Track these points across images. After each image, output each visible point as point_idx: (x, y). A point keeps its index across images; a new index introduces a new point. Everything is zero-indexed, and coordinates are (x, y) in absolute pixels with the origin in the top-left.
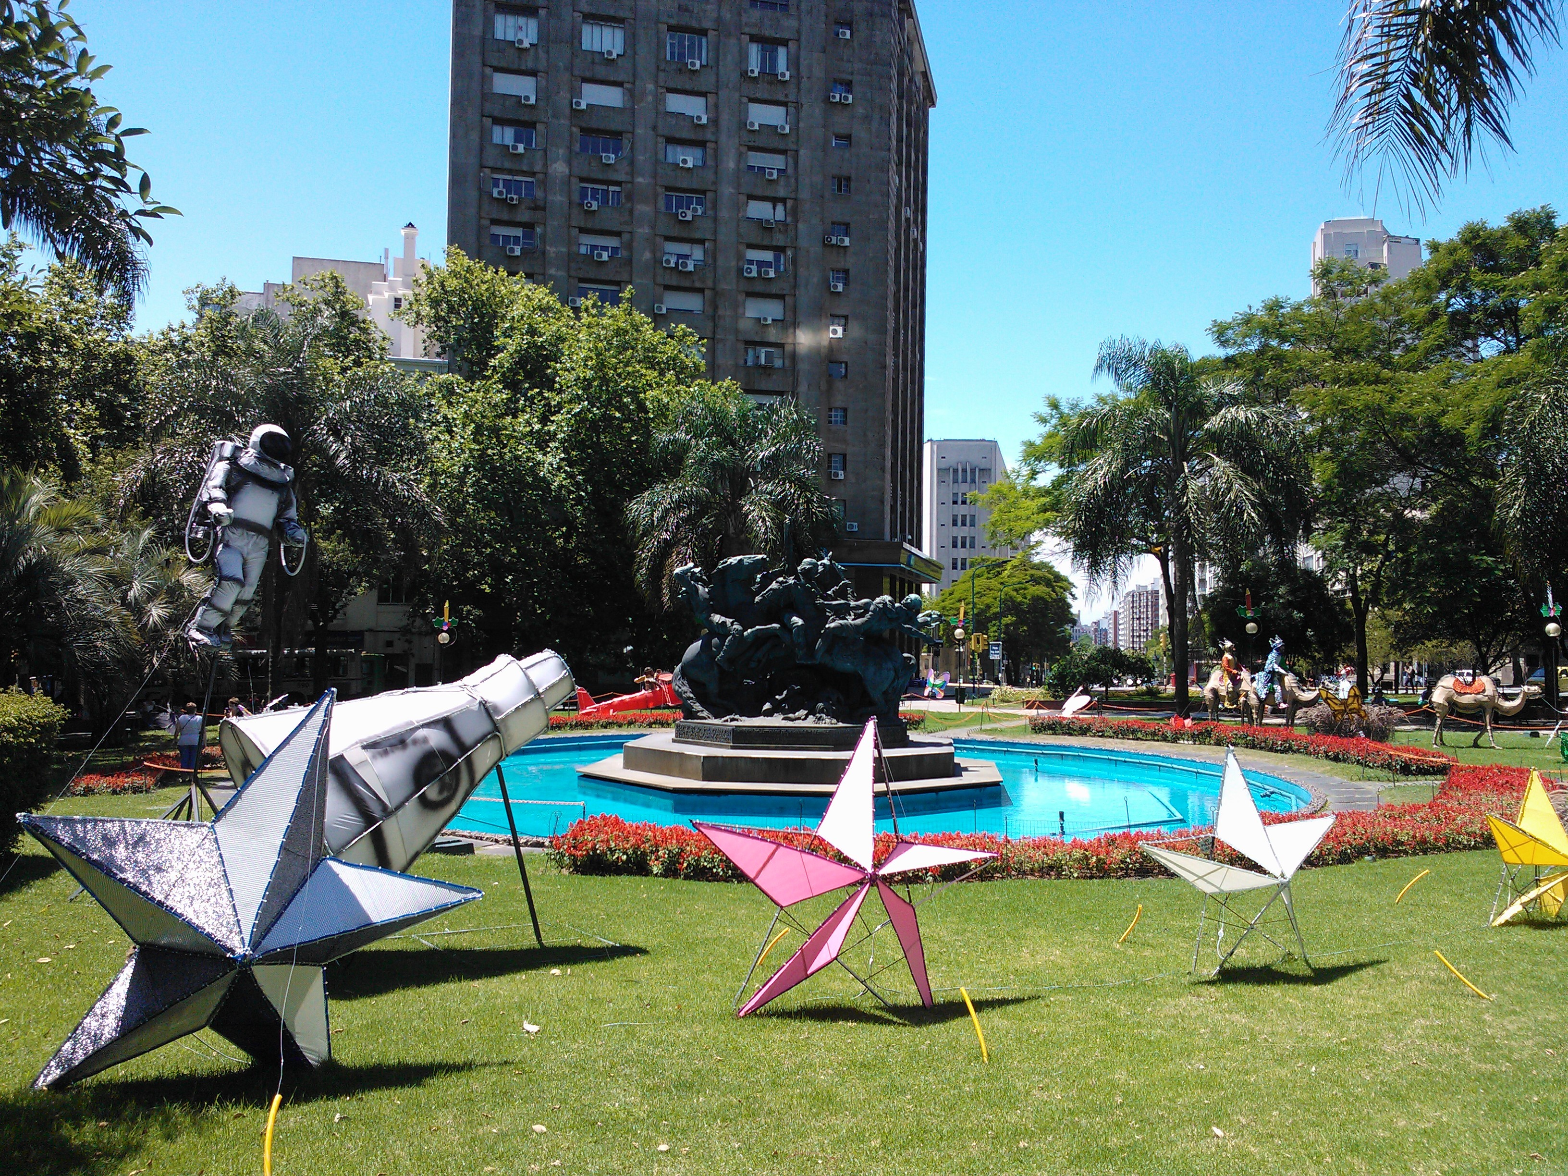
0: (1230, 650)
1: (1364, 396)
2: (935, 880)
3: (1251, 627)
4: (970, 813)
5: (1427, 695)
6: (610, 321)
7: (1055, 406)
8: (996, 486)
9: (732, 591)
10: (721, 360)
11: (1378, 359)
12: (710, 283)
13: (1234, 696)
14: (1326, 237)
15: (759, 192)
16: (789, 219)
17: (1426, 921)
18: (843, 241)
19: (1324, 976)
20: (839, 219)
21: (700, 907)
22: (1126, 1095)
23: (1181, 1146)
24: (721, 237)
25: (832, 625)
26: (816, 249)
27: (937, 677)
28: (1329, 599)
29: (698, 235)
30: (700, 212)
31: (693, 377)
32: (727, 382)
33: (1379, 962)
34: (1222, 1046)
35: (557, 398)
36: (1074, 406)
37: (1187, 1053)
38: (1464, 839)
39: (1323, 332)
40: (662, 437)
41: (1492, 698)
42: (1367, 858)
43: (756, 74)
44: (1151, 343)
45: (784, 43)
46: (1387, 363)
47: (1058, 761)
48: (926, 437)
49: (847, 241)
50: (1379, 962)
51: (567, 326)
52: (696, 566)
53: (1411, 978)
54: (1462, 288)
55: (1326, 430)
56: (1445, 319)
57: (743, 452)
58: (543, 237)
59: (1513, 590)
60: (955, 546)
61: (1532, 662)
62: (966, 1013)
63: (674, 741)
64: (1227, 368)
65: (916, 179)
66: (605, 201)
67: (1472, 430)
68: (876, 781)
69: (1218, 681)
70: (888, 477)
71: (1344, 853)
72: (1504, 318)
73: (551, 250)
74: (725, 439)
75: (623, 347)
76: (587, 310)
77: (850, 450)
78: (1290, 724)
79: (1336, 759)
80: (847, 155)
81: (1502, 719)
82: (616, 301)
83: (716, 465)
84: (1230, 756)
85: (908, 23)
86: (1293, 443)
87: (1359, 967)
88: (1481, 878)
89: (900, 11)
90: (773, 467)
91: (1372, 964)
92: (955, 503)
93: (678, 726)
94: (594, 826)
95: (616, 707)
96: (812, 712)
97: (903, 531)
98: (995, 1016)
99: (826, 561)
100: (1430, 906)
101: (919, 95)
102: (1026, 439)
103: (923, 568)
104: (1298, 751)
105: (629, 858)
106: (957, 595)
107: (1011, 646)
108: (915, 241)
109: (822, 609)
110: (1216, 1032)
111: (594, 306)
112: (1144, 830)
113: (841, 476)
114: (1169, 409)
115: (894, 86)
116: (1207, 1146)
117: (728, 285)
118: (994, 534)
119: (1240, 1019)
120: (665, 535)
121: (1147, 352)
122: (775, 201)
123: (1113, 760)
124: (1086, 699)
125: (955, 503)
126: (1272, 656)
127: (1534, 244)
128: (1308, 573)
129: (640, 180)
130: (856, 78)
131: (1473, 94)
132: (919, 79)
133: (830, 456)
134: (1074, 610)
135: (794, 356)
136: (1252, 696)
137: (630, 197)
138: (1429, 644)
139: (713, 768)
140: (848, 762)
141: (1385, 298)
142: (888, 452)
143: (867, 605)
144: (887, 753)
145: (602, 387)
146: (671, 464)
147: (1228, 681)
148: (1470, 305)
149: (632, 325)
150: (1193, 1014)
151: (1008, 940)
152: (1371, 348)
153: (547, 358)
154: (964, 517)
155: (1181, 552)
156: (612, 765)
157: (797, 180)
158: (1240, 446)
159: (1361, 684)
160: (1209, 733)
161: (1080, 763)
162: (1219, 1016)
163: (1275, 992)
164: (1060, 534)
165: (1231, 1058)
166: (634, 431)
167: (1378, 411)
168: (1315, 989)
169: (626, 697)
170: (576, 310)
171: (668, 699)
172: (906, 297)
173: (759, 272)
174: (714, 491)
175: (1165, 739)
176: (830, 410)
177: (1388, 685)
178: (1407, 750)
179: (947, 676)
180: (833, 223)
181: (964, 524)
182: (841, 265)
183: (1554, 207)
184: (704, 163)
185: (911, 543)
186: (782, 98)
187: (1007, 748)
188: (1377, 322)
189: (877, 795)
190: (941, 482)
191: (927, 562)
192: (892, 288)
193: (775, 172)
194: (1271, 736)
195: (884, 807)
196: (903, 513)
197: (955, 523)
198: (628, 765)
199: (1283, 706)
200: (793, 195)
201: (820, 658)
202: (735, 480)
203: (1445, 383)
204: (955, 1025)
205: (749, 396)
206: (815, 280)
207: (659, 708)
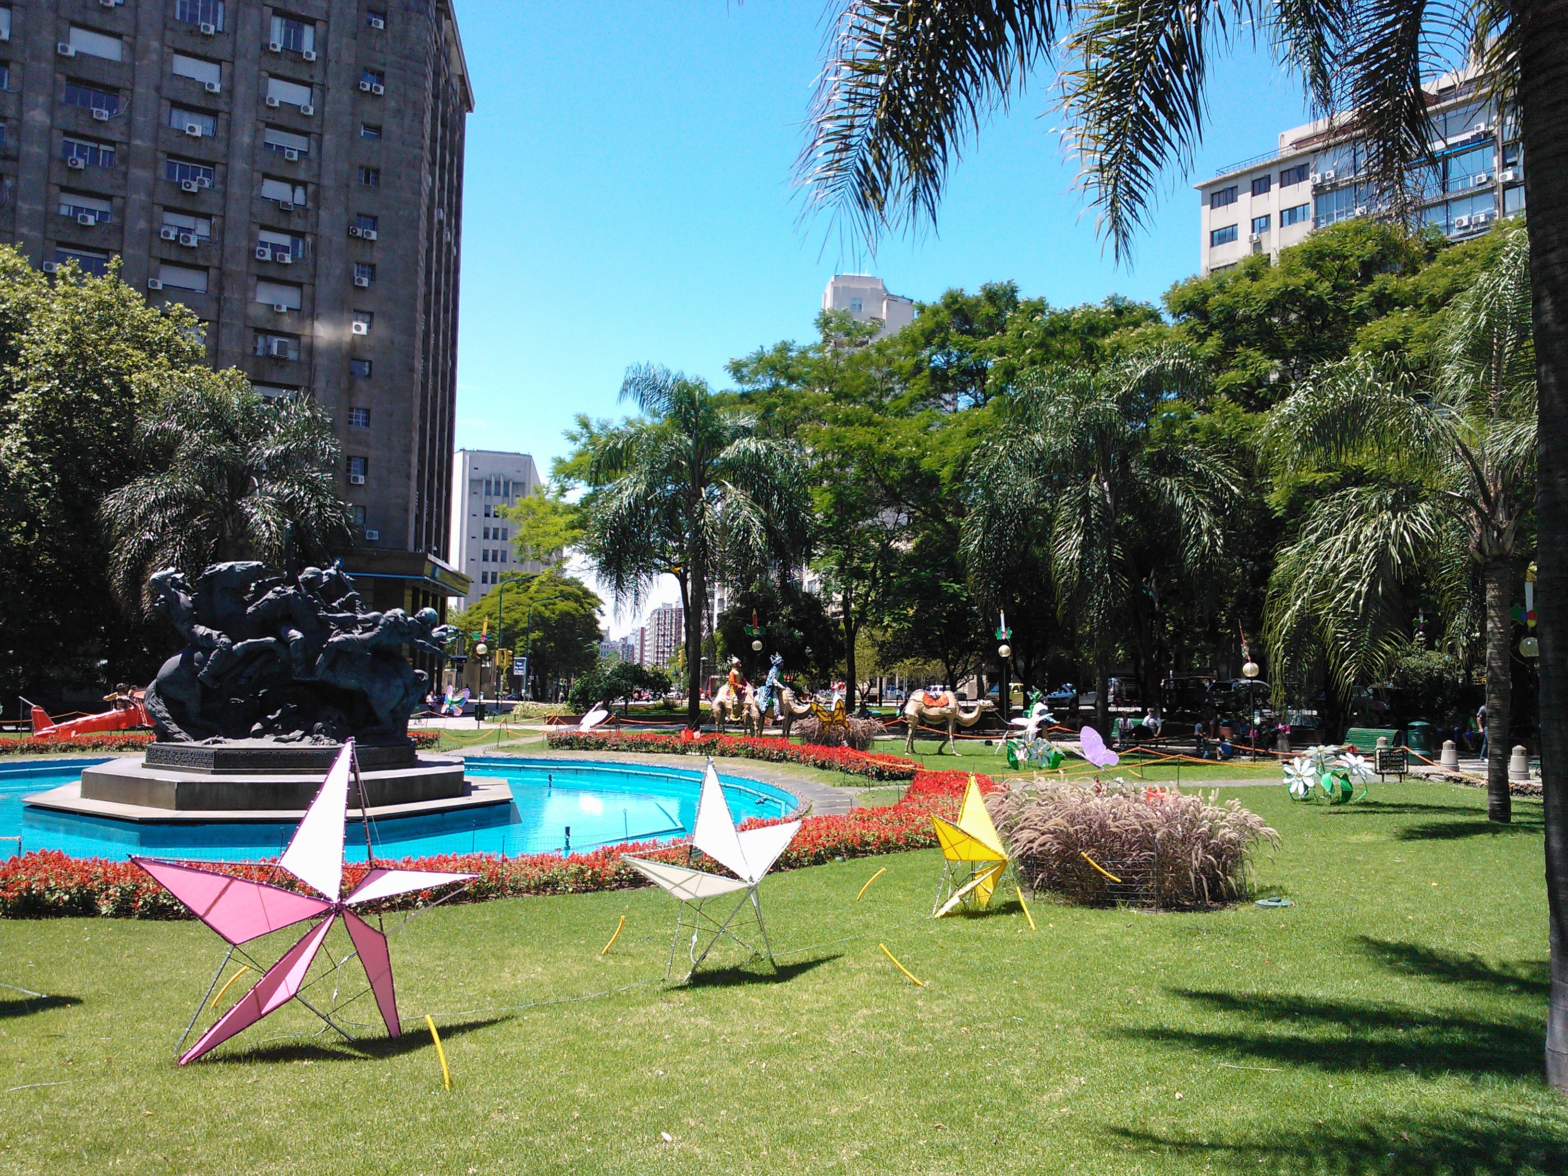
0: (736, 666)
1: (858, 436)
2: (426, 904)
3: (757, 644)
4: (470, 833)
5: (902, 708)
6: (91, 293)
7: (585, 425)
8: (524, 501)
9: (220, 601)
10: (225, 346)
11: (871, 404)
12: (215, 262)
13: (739, 708)
14: (836, 290)
15: (276, 172)
16: (310, 205)
17: (880, 916)
18: (369, 234)
19: (785, 973)
20: (364, 210)
21: (152, 949)
22: (584, 1108)
23: (630, 1154)
24: (230, 214)
25: (336, 639)
26: (340, 239)
27: (456, 693)
28: (825, 620)
29: (203, 209)
30: (207, 185)
31: (191, 362)
32: (231, 371)
33: (835, 957)
34: (684, 1050)
35: (21, 374)
36: (604, 427)
37: (649, 1061)
38: (921, 838)
39: (826, 375)
40: (149, 425)
41: (954, 711)
42: (838, 858)
43: (278, 49)
44: (674, 372)
45: (312, 22)
46: (879, 408)
47: (573, 776)
48: (457, 447)
49: (374, 235)
50: (835, 957)
51: (39, 293)
52: (177, 572)
53: (861, 970)
54: (942, 346)
55: (825, 466)
56: (927, 372)
57: (245, 448)
58: (14, 191)
59: (977, 616)
60: (485, 559)
61: (992, 679)
62: (431, 1041)
63: (144, 766)
64: (742, 403)
65: (451, 181)
66: (94, 158)
67: (946, 473)
68: (349, 806)
69: (725, 695)
70: (414, 484)
71: (818, 855)
72: (973, 376)
73: (24, 207)
74: (225, 432)
75: (104, 324)
76: (64, 277)
77: (372, 454)
78: (786, 735)
79: (823, 767)
80: (377, 146)
81: (962, 730)
82: (100, 272)
83: (212, 461)
84: (710, 767)
85: (445, 24)
86: (796, 474)
87: (818, 962)
88: (931, 873)
89: (437, 9)
90: (279, 468)
91: (828, 959)
92: (487, 515)
93: (149, 750)
94: (31, 863)
95: (79, 729)
96: (308, 732)
97: (428, 541)
98: (464, 1043)
99: (332, 571)
100: (887, 901)
101: (453, 101)
102: (556, 455)
103: (449, 580)
104: (791, 760)
105: (72, 899)
106: (484, 610)
107: (538, 662)
108: (449, 244)
109: (326, 621)
110: (680, 1036)
111: (73, 274)
112: (641, 842)
113: (361, 480)
114: (690, 437)
115: (429, 84)
116: (655, 1152)
117: (237, 266)
118: (522, 549)
119: (704, 1022)
120: (148, 536)
121: (670, 381)
122: (294, 183)
123: (626, 773)
124: (604, 714)
125: (487, 515)
126: (773, 671)
127: (1000, 314)
128: (809, 595)
129: (138, 142)
130: (388, 71)
131: (927, 176)
132: (456, 82)
133: (349, 458)
134: (601, 627)
135: (311, 350)
136: (754, 709)
137: (124, 159)
138: (907, 662)
139: (188, 795)
140: (319, 786)
141: (879, 350)
142: (415, 460)
143: (377, 618)
144: (364, 776)
145: (77, 363)
146: (159, 456)
147: (733, 695)
148: (947, 362)
149: (117, 298)
150: (662, 1020)
151: (492, 961)
152: (865, 394)
153: (9, 327)
154: (496, 530)
155: (696, 573)
156: (68, 794)
157: (320, 166)
158: (751, 474)
159: (850, 698)
160: (714, 744)
161: (594, 777)
162: (685, 1021)
163: (739, 992)
164: (587, 552)
165: (690, 1062)
166: (115, 416)
167: (870, 451)
168: (776, 986)
169: (93, 717)
170: (51, 277)
171: (144, 718)
172: (437, 302)
173: (274, 256)
174: (208, 490)
175: (675, 751)
176: (351, 410)
177: (873, 699)
178: (882, 758)
179: (466, 693)
180: (359, 215)
181: (495, 537)
182: (367, 259)
183: (1017, 282)
184: (215, 132)
185: (437, 554)
186: (307, 78)
187: (522, 765)
188: (872, 371)
189: (349, 821)
190: (473, 493)
191: (455, 575)
192: (422, 290)
193: (296, 154)
194: (768, 747)
195: (355, 832)
196: (429, 525)
197: (486, 536)
198: (86, 793)
199: (780, 718)
200: (315, 180)
201: (320, 674)
202: (238, 479)
203: (925, 429)
204: (419, 1055)
205: (256, 388)
206: (338, 271)
207: (133, 729)
